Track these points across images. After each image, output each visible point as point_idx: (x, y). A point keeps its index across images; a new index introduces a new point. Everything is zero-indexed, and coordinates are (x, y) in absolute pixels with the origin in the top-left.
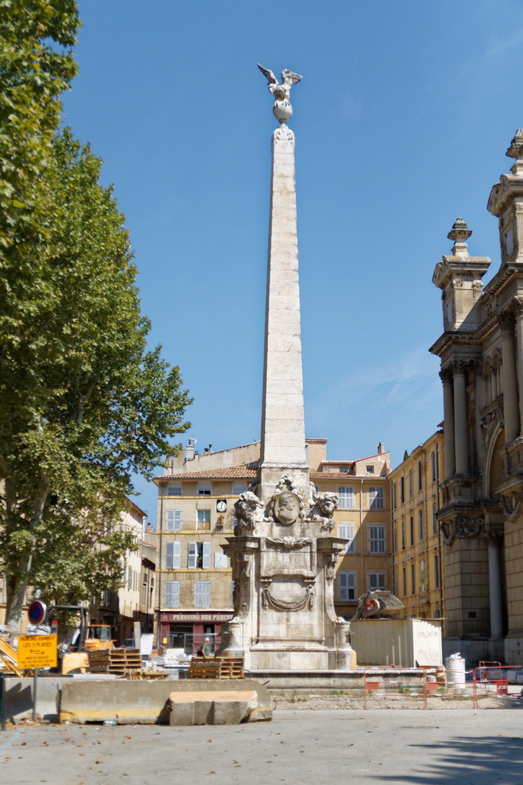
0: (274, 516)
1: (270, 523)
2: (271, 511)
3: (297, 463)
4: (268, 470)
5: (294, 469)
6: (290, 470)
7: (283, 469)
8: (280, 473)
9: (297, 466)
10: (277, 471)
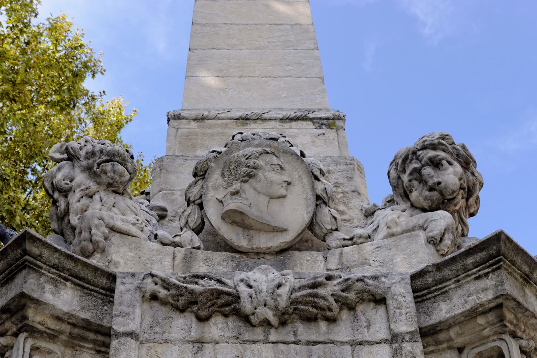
1: (180, 252)
3: (463, 284)
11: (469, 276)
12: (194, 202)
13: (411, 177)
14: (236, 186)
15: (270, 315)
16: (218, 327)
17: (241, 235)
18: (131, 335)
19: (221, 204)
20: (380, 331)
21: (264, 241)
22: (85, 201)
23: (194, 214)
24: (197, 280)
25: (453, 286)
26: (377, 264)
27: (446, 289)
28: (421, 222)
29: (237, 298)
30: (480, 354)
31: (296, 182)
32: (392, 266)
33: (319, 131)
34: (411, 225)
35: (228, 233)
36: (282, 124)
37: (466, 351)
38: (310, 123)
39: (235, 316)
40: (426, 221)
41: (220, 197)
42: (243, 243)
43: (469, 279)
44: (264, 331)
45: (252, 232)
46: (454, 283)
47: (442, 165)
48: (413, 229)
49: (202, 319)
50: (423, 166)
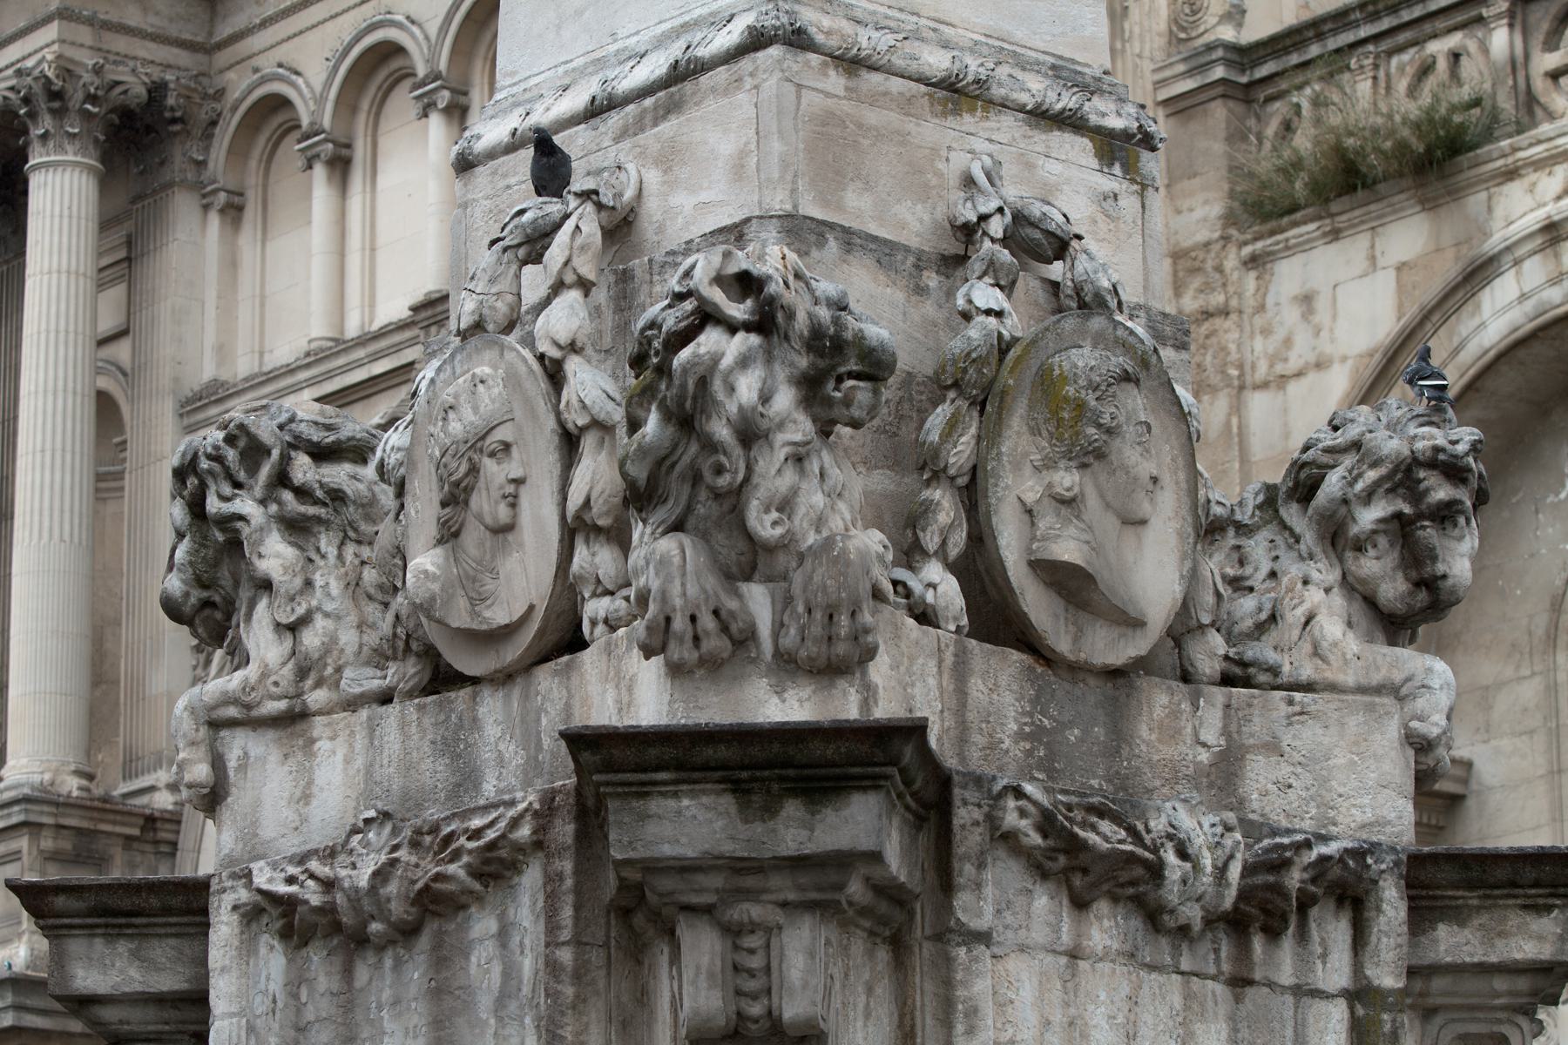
0: (977, 568)
2: (945, 506)
4: (835, 81)
5: (1041, 117)
6: (1007, 126)
7: (957, 94)
8: (932, 131)
9: (1067, 101)
10: (906, 105)
11: (1515, 897)
12: (953, 479)
13: (1382, 526)
14: (1066, 479)
15: (1193, 914)
16: (1106, 929)
17: (1062, 621)
18: (984, 938)
19: (1026, 517)
20: (1335, 973)
21: (1107, 648)
22: (789, 477)
23: (960, 525)
24: (1094, 819)
25: (1475, 902)
26: (1297, 757)
27: (1460, 902)
28: (1398, 677)
29: (1156, 871)
30: (1463, 1037)
31: (1166, 479)
32: (1324, 773)
33: (1107, 184)
34: (1376, 678)
35: (1037, 604)
36: (1030, 133)
37: (1439, 1020)
38: (1085, 143)
39: (1130, 905)
40: (1408, 680)
41: (1030, 498)
42: (1062, 644)
43: (1511, 902)
44: (1173, 945)
45: (1084, 617)
46: (1479, 897)
47: (1456, 525)
48: (1378, 690)
49: (1080, 904)
50: (1420, 516)
